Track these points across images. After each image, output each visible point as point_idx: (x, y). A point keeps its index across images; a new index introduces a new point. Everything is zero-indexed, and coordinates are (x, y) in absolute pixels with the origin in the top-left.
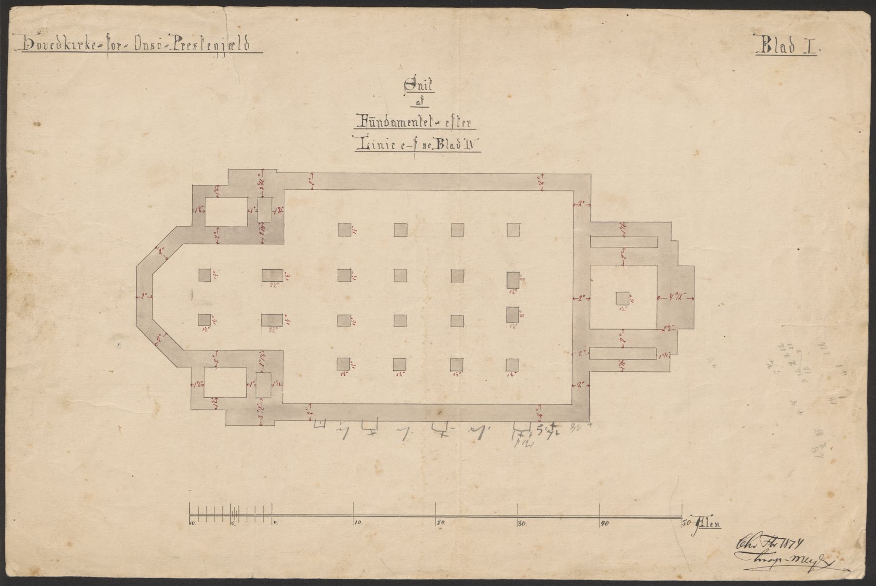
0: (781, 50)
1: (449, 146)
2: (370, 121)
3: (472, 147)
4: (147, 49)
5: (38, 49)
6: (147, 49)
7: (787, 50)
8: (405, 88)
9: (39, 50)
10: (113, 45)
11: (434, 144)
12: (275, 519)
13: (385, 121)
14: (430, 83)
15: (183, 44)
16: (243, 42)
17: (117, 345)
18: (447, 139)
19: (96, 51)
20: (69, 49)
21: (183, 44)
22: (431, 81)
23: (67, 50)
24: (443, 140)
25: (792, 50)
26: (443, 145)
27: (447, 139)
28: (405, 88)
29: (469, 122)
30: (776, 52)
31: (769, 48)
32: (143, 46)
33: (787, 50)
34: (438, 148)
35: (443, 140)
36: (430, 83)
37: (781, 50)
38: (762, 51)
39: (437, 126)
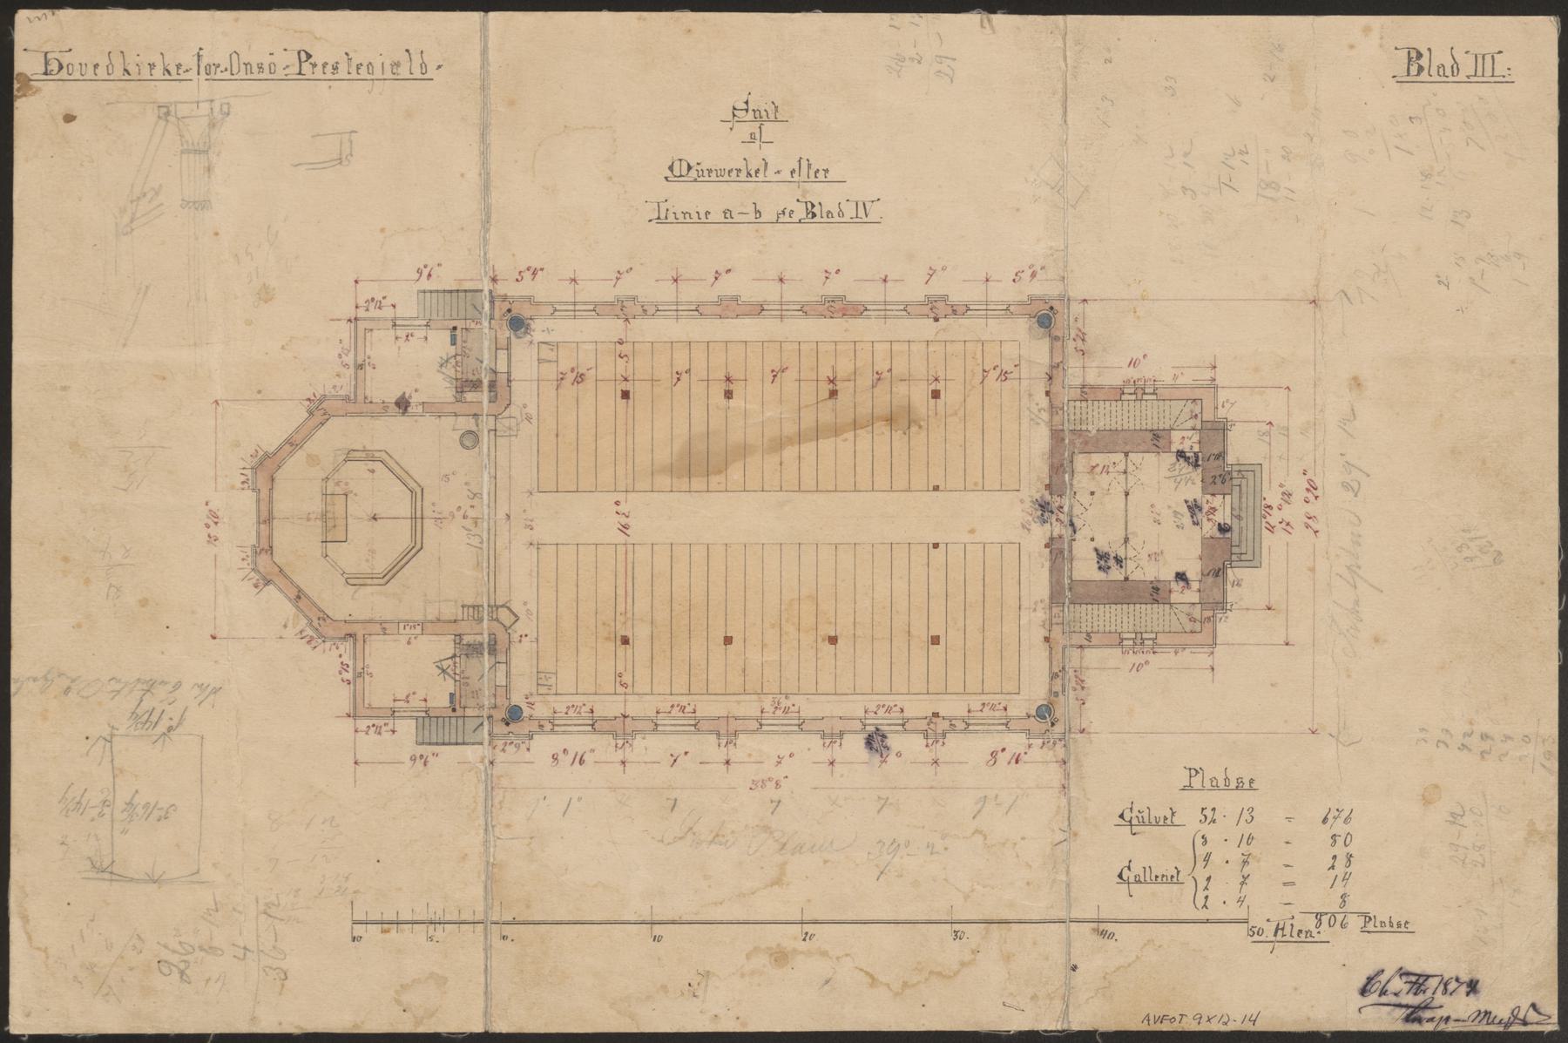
0: (1438, 72)
1: (824, 215)
2: (697, 170)
3: (867, 216)
4: (251, 73)
5: (108, 74)
6: (251, 73)
7: (1448, 72)
8: (734, 115)
9: (423, 77)
10: (371, 68)
11: (800, 212)
12: (658, 930)
13: (1452, 67)
14: (776, 111)
15: (315, 65)
16: (417, 59)
17: (1288, 488)
18: (820, 204)
19: (363, 78)
20: (129, 74)
21: (315, 65)
22: (776, 107)
23: (127, 77)
24: (813, 206)
25: (110, 72)
26: (1421, 69)
27: (820, 204)
28: (734, 115)
29: (826, 171)
30: (411, 74)
31: (1421, 69)
32: (243, 67)
33: (1448, 72)
34: (1408, 75)
35: (813, 206)
36: (776, 111)
37: (1438, 72)
38: (298, 72)
39: (778, 178)
